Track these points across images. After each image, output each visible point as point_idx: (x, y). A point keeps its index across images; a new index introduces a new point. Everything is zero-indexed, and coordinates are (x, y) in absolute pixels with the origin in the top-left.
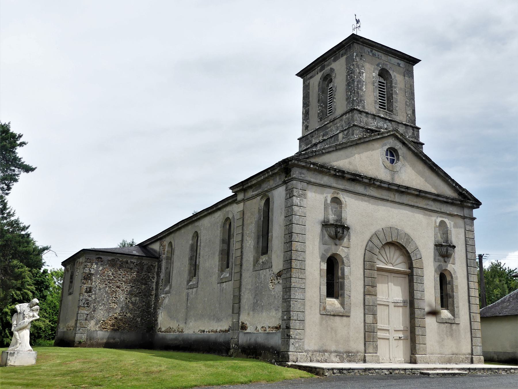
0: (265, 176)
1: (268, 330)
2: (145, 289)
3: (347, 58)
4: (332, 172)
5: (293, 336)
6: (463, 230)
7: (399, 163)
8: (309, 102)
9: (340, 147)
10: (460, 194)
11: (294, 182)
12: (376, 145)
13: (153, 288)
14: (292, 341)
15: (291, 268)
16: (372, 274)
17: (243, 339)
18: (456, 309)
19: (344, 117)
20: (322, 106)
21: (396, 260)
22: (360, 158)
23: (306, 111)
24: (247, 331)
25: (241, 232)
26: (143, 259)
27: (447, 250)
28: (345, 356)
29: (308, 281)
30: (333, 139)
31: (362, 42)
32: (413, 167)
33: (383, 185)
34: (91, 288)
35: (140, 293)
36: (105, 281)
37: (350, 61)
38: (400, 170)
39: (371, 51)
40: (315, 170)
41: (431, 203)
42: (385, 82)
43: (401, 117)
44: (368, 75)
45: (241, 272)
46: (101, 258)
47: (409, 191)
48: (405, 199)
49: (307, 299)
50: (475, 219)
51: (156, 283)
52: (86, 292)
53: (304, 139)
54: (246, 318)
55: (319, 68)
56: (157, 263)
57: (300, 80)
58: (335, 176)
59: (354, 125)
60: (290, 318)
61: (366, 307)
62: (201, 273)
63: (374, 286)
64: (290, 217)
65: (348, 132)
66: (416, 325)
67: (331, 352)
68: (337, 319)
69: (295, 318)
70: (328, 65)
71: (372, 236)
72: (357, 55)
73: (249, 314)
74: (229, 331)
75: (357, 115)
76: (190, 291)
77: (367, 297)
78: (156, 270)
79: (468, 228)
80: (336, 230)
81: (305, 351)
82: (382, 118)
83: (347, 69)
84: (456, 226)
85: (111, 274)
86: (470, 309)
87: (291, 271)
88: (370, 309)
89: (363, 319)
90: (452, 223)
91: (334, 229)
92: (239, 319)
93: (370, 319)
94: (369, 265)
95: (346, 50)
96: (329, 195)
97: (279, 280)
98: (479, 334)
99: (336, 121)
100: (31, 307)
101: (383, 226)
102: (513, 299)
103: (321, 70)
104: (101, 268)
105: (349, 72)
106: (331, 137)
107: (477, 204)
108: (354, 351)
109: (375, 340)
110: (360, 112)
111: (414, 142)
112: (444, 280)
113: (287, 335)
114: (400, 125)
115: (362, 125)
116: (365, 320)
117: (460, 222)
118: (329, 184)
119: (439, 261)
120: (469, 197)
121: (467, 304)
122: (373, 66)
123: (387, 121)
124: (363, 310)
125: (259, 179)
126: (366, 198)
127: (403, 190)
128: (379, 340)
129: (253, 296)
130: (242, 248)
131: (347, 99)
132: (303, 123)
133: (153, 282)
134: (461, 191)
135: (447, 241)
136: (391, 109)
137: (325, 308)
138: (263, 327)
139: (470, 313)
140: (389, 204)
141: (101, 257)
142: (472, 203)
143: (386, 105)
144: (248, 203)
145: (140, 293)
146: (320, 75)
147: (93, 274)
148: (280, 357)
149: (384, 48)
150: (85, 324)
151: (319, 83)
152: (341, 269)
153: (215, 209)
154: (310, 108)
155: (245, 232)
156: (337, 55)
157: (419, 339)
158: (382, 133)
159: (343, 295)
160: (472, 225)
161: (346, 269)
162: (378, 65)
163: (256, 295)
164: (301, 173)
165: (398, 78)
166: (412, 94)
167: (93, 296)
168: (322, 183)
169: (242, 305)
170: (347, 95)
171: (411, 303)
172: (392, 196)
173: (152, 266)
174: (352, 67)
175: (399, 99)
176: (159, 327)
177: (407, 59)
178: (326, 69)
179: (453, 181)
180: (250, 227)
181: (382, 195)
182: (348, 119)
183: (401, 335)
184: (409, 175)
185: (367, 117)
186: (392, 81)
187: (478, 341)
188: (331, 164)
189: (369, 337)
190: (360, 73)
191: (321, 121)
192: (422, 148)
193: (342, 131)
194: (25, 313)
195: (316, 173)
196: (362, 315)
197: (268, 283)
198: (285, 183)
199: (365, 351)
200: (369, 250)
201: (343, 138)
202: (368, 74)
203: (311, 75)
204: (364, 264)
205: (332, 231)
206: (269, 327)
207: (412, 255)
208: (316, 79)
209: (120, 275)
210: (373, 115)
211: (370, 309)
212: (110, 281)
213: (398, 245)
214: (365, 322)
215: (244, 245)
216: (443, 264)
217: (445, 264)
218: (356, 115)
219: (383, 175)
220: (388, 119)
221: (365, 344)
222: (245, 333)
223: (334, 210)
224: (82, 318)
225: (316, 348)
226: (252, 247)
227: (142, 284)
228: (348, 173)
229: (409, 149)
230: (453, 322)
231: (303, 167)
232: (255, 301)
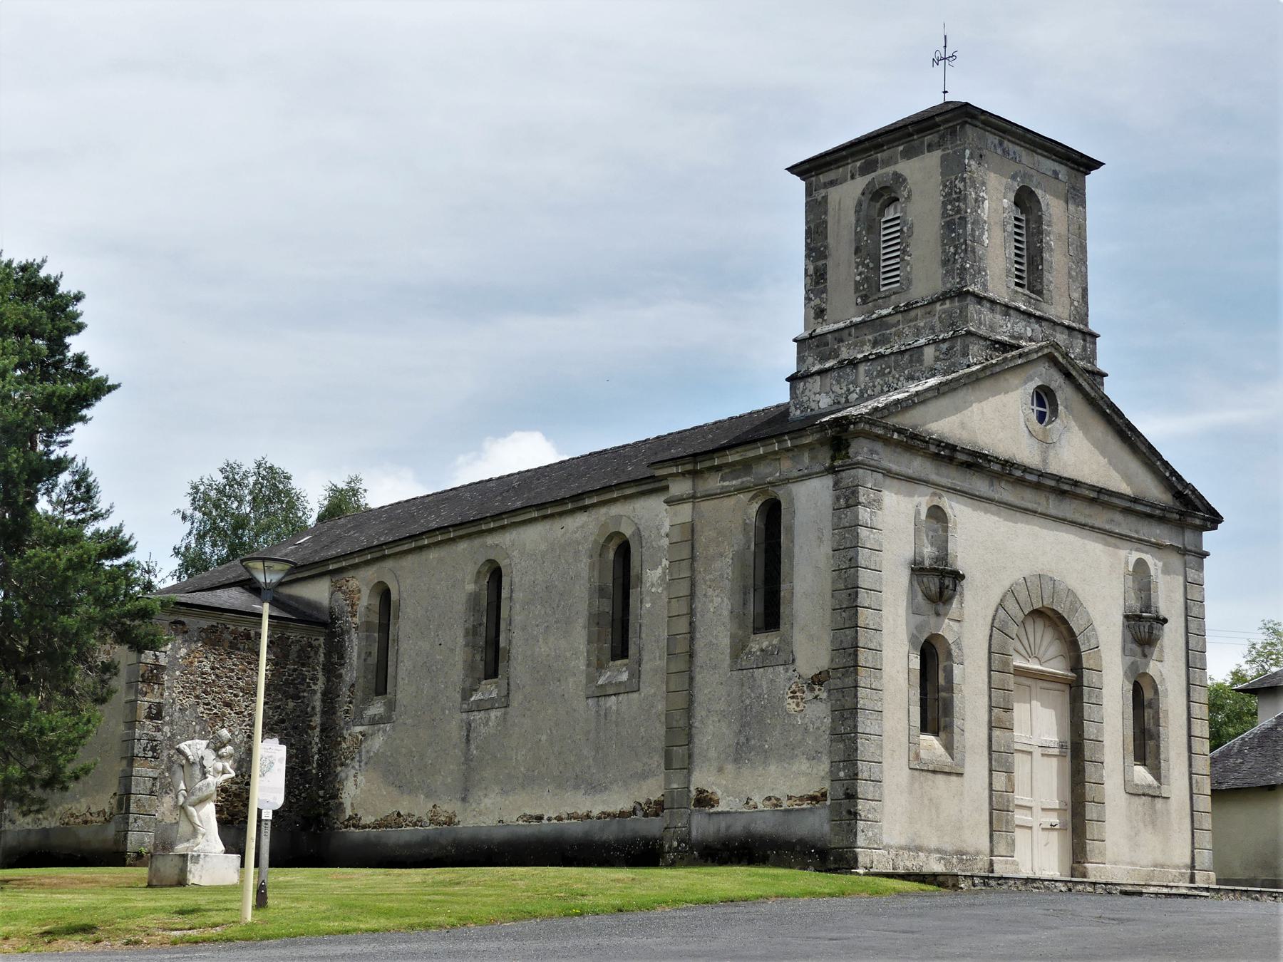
0: (770, 449)
1: (786, 804)
2: (294, 710)
3: (944, 159)
4: (933, 449)
5: (863, 814)
6: (1181, 579)
7: (1057, 424)
8: (826, 248)
9: (946, 388)
10: (1178, 495)
11: (861, 471)
12: (1013, 379)
13: (313, 708)
14: (861, 824)
15: (856, 666)
16: (1007, 682)
17: (701, 827)
18: (1163, 764)
19: (938, 307)
20: (867, 266)
21: (1046, 651)
22: (982, 413)
23: (816, 270)
24: (719, 809)
25: (687, 574)
26: (287, 628)
27: (1151, 628)
28: (954, 861)
29: (886, 695)
30: (907, 356)
31: (984, 122)
32: (1084, 428)
33: (1028, 477)
34: (159, 706)
35: (283, 721)
36: (194, 689)
37: (952, 167)
38: (1059, 440)
39: (1001, 144)
40: (898, 444)
41: (1118, 517)
42: (1023, 217)
43: (1058, 309)
44: (994, 205)
45: (690, 670)
46: (183, 623)
47: (1078, 491)
48: (1069, 509)
49: (885, 734)
50: (1206, 554)
51: (324, 694)
52: (149, 717)
53: (814, 342)
54: (711, 779)
55: (858, 164)
56: (322, 640)
57: (799, 185)
58: (936, 457)
59: (969, 333)
60: (857, 774)
61: (994, 755)
62: (518, 667)
63: (1008, 709)
64: (851, 553)
65: (951, 348)
66: (1088, 798)
67: (930, 851)
68: (940, 777)
69: (866, 775)
70: (887, 163)
71: (1004, 596)
72: (971, 157)
73: (720, 770)
74: (634, 812)
75: (973, 308)
76: (478, 716)
77: (996, 733)
78: (322, 659)
79: (1192, 574)
80: (938, 582)
81: (884, 848)
82: (1024, 313)
83: (945, 186)
84: (1166, 571)
85: (208, 669)
86: (1190, 765)
87: (856, 673)
88: (1000, 759)
89: (987, 780)
90: (1160, 564)
91: (937, 580)
92: (689, 782)
93: (1000, 781)
94: (996, 661)
95: (943, 137)
96: (923, 500)
97: (817, 692)
98: (1206, 822)
99: (913, 313)
100: (216, 750)
101: (1026, 573)
102: (1251, 749)
103: (864, 171)
104: (183, 652)
105: (950, 194)
106: (902, 352)
107: (1214, 519)
108: (971, 850)
109: (1010, 828)
110: (980, 299)
111: (1088, 372)
112: (1142, 698)
113: (849, 812)
114: (1058, 328)
115: (983, 331)
116: (991, 784)
117: (1176, 560)
118: (923, 476)
119: (1133, 654)
120: (1198, 503)
121: (1186, 754)
122: (1004, 180)
123: (1033, 320)
124: (987, 762)
125: (751, 454)
126: (994, 508)
127: (1066, 487)
128: (1018, 831)
129: (736, 728)
130: (692, 613)
131: (945, 263)
132: (808, 299)
133: (315, 692)
134: (1180, 488)
135: (1148, 607)
136: (1039, 287)
137: (917, 756)
138: (769, 799)
139: (1191, 773)
140: (1036, 519)
141: (182, 619)
142: (1204, 519)
143: (1025, 275)
144: (706, 506)
145: (283, 721)
146: (861, 183)
147: (163, 668)
148: (833, 857)
149: (1029, 136)
150: (150, 806)
151: (860, 204)
152: (945, 671)
153: (570, 506)
154: (830, 263)
155: (699, 577)
156: (916, 143)
157: (1092, 830)
158: (1027, 354)
159: (949, 728)
160: (1200, 568)
161: (957, 670)
162: (1014, 178)
163: (743, 726)
164: (872, 452)
165: (1053, 207)
166: (1083, 248)
167: (166, 729)
168: (910, 472)
169: (696, 751)
170: (944, 251)
171: (1077, 752)
172: (1043, 500)
173: (311, 646)
174: (961, 186)
175: (1056, 260)
176: (349, 813)
177: (1074, 161)
178: (880, 172)
179: (1166, 464)
180: (717, 564)
181: (1023, 498)
182: (950, 314)
183: (1055, 820)
184: (1079, 453)
185: (992, 310)
186: (1041, 217)
187: (1205, 839)
188: (928, 427)
189: (999, 820)
190: (979, 201)
191: (864, 302)
192: (1103, 384)
193: (935, 342)
194: (205, 763)
195: (899, 450)
196: (986, 773)
197: (782, 699)
198: (832, 470)
199: (992, 851)
200: (996, 627)
201: (937, 359)
202: (993, 202)
203: (831, 175)
204: (990, 659)
205: (933, 584)
206: (790, 798)
207: (1080, 639)
208: (847, 193)
209: (232, 671)
210: (1007, 306)
211: (1000, 759)
212: (207, 688)
213: (1054, 619)
214: (991, 790)
215: (698, 606)
216: (1139, 659)
217: (1144, 661)
218: (971, 308)
219: (1024, 451)
220: (1035, 316)
221: (991, 836)
222: (710, 814)
223: (931, 534)
224: (141, 789)
225: (902, 841)
226: (726, 613)
227: (287, 696)
228: (963, 450)
229: (1079, 388)
230: (1157, 793)
231: (877, 437)
232: (742, 739)
